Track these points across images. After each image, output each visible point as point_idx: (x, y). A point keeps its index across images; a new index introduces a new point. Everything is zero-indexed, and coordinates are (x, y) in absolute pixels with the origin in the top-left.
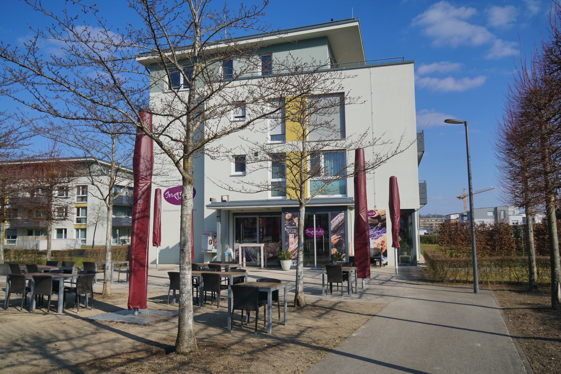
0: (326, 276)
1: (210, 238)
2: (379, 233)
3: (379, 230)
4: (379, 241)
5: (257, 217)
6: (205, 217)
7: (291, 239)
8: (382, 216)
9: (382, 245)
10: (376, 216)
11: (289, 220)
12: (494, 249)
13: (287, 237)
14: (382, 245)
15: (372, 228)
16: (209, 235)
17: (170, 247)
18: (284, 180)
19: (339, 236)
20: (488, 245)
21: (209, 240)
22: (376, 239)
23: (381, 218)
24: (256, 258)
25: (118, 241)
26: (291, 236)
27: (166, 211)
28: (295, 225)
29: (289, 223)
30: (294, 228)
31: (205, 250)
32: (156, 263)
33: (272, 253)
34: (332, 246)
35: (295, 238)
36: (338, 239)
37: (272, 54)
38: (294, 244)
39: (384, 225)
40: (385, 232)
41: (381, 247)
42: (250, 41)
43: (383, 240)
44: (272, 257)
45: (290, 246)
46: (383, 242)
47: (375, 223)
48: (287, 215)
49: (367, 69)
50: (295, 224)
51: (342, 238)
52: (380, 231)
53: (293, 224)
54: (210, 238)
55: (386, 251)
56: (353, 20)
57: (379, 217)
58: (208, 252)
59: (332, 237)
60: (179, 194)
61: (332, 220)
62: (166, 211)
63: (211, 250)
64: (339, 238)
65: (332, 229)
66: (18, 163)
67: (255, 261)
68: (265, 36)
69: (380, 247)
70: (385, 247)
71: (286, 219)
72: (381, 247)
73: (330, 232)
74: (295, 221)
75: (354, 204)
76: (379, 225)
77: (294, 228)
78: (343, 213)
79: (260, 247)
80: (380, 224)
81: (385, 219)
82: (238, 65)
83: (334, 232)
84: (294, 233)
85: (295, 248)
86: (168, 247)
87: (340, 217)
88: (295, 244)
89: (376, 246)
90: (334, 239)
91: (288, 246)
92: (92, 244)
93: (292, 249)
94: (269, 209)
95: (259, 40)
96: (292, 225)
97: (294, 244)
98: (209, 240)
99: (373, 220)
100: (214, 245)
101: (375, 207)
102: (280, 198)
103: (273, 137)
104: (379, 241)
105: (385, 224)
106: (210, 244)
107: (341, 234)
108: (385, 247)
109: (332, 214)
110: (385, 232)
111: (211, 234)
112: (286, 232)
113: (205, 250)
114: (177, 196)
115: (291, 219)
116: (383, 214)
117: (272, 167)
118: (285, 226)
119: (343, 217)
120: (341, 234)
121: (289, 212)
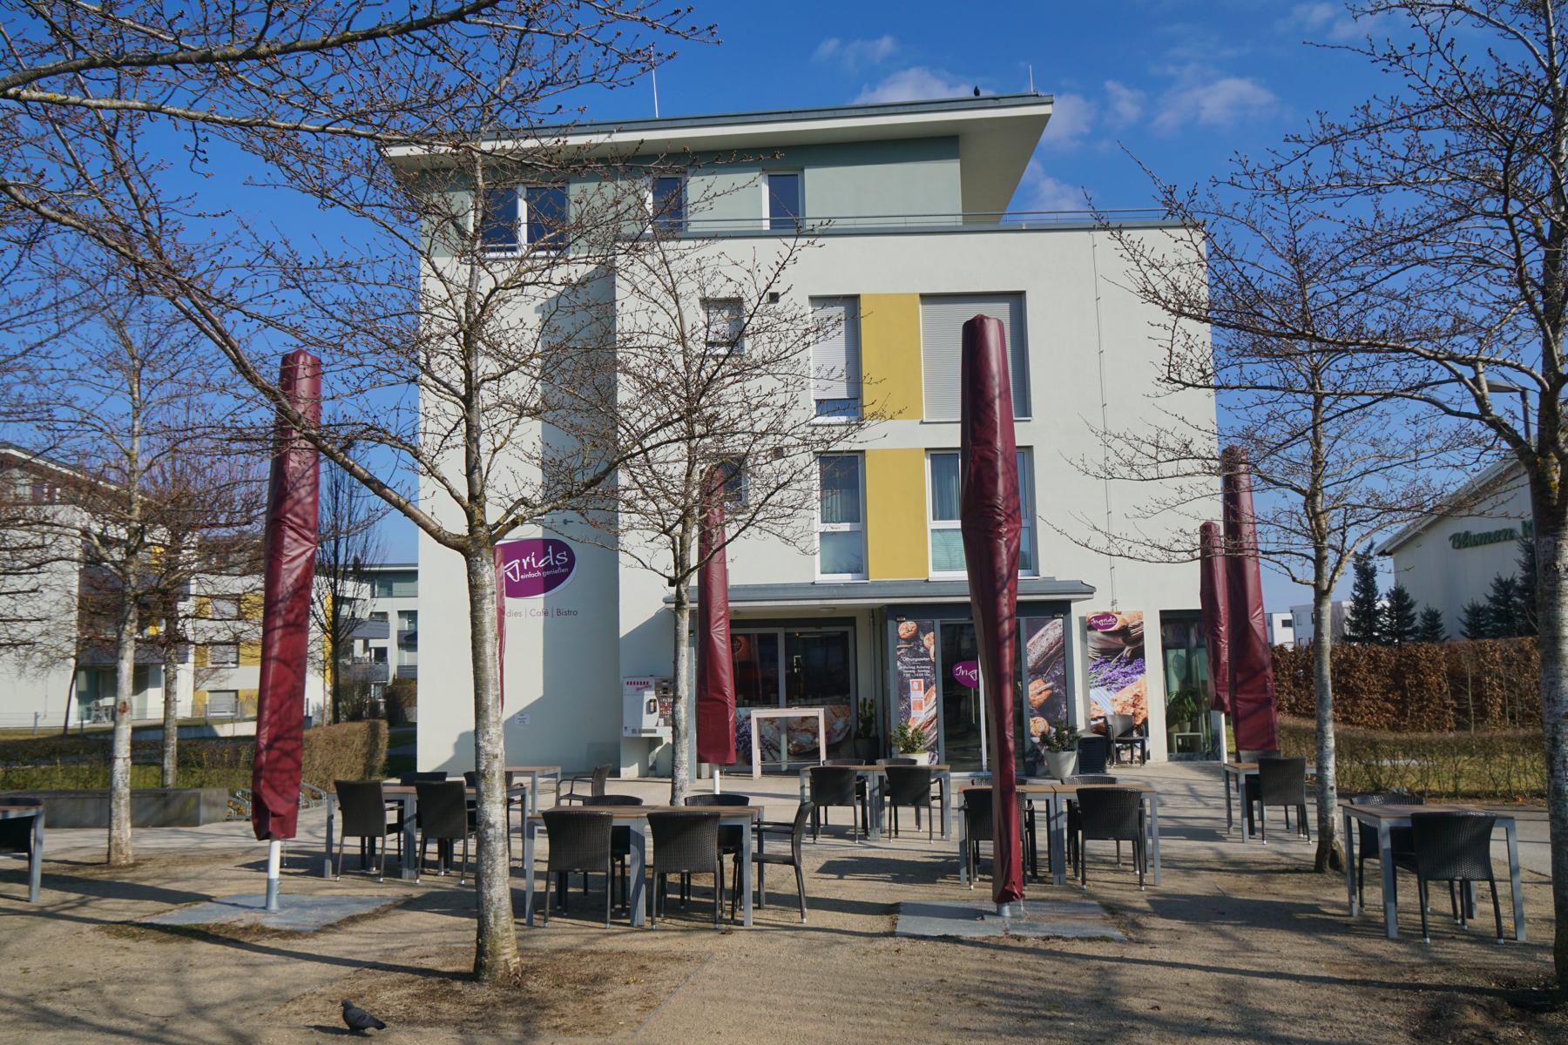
0: (338, 817)
1: (650, 695)
2: (1125, 674)
3: (1126, 664)
5: (781, 633)
7: (917, 692)
8: (1134, 627)
9: (1134, 705)
10: (1116, 627)
11: (908, 640)
12: (1402, 713)
13: (905, 689)
14: (1134, 705)
16: (647, 686)
18: (857, 526)
19: (1050, 684)
20: (1387, 700)
21: (646, 699)
22: (1118, 689)
23: (1129, 634)
24: (779, 751)
25: (94, 713)
26: (916, 685)
28: (926, 654)
29: (910, 649)
30: (923, 663)
31: (634, 731)
34: (1031, 711)
35: (926, 691)
36: (1048, 692)
37: (803, 170)
39: (1139, 653)
40: (1142, 672)
41: (1132, 710)
43: (1136, 691)
45: (914, 713)
46: (1137, 697)
47: (1114, 647)
48: (902, 626)
49: (1085, 234)
50: (927, 650)
51: (1059, 687)
52: (1128, 669)
53: (922, 650)
54: (650, 695)
55: (1145, 721)
56: (1032, 100)
57: (1124, 631)
58: (643, 735)
59: (1031, 687)
60: (521, 565)
61: (1029, 638)
63: (655, 731)
64: (1051, 688)
65: (1030, 665)
66: (66, 471)
67: (775, 759)
69: (1130, 711)
70: (1144, 712)
71: (899, 637)
72: (1132, 710)
73: (1025, 674)
74: (926, 643)
76: (1127, 651)
77: (923, 663)
79: (758, 719)
80: (1127, 648)
81: (1141, 637)
82: (584, 196)
83: (1037, 672)
84: (924, 677)
85: (928, 719)
87: (1050, 632)
88: (928, 708)
90: (1036, 690)
91: (908, 712)
92: (63, 724)
93: (919, 723)
94: (834, 608)
98: (646, 699)
99: (1110, 639)
101: (1113, 603)
102: (847, 578)
103: (824, 406)
105: (1142, 648)
106: (649, 712)
107: (1056, 679)
108: (1144, 712)
109: (1029, 624)
110: (1142, 672)
111: (652, 682)
112: (900, 673)
113: (634, 731)
114: (513, 572)
115: (914, 639)
116: (1136, 623)
117: (822, 491)
118: (899, 658)
119: (1059, 631)
120: (1056, 679)
121: (909, 618)
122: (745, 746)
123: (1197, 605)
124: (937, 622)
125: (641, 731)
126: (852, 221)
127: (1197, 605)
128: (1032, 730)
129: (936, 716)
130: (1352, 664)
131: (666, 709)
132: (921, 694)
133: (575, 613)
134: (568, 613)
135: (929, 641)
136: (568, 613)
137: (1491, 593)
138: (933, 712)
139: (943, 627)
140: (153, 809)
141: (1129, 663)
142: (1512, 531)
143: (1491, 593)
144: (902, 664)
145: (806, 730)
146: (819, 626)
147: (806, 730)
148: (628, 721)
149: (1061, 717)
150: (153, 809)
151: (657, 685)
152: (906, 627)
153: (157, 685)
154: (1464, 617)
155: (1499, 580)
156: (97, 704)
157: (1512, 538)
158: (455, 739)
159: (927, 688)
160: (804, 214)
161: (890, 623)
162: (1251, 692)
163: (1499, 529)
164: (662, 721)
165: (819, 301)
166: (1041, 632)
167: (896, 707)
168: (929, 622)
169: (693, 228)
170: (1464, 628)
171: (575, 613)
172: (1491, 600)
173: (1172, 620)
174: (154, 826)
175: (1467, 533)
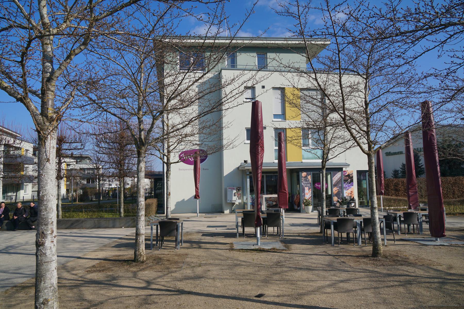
2: (349, 186)
3: (349, 183)
4: (349, 191)
6: (224, 175)
9: (351, 194)
11: (305, 177)
14: (351, 194)
15: (345, 183)
16: (234, 189)
17: (186, 200)
21: (234, 193)
22: (347, 190)
25: (6, 198)
26: (306, 189)
27: (181, 170)
28: (309, 181)
30: (308, 183)
31: (230, 201)
32: (197, 213)
33: (275, 202)
37: (266, 53)
38: (309, 195)
39: (352, 181)
40: (353, 185)
42: (277, 42)
44: (275, 205)
45: (306, 196)
50: (309, 180)
52: (349, 185)
57: (349, 175)
62: (181, 170)
64: (338, 189)
65: (333, 184)
68: (256, 40)
74: (309, 178)
75: (277, 167)
76: (349, 180)
77: (308, 183)
78: (340, 173)
81: (352, 177)
83: (335, 185)
86: (184, 200)
89: (347, 195)
91: (304, 196)
95: (285, 42)
96: (307, 181)
97: (309, 195)
98: (234, 193)
99: (345, 177)
100: (237, 197)
104: (349, 191)
105: (353, 179)
106: (235, 196)
111: (235, 188)
112: (303, 186)
113: (230, 201)
115: (306, 177)
121: (305, 172)
122: (330, 201)
123: (367, 169)
124: (312, 173)
125: (232, 201)
126: (242, 66)
127: (367, 169)
128: (334, 200)
129: (311, 197)
130: (398, 184)
131: (239, 195)
132: (308, 191)
133: (208, 169)
134: (206, 169)
135: (310, 177)
136: (206, 169)
137: (401, 167)
138: (311, 195)
139: (313, 174)
140: (130, 223)
141: (350, 183)
142: (402, 152)
143: (401, 167)
144: (303, 183)
145: (271, 200)
146: (274, 174)
147: (271, 200)
148: (229, 198)
149: (341, 197)
150: (130, 223)
151: (237, 189)
152: (304, 174)
153: (23, 189)
154: (393, 172)
155: (403, 164)
156: (7, 195)
157: (402, 154)
158: (175, 204)
159: (309, 189)
160: (237, 64)
161: (300, 173)
162: (412, 190)
163: (399, 151)
164: (238, 198)
165: (274, 88)
166: (336, 175)
167: (302, 194)
168: (309, 173)
169: (238, 67)
170: (392, 175)
171: (208, 169)
172: (401, 168)
173: (360, 173)
174: (131, 227)
175: (390, 152)
